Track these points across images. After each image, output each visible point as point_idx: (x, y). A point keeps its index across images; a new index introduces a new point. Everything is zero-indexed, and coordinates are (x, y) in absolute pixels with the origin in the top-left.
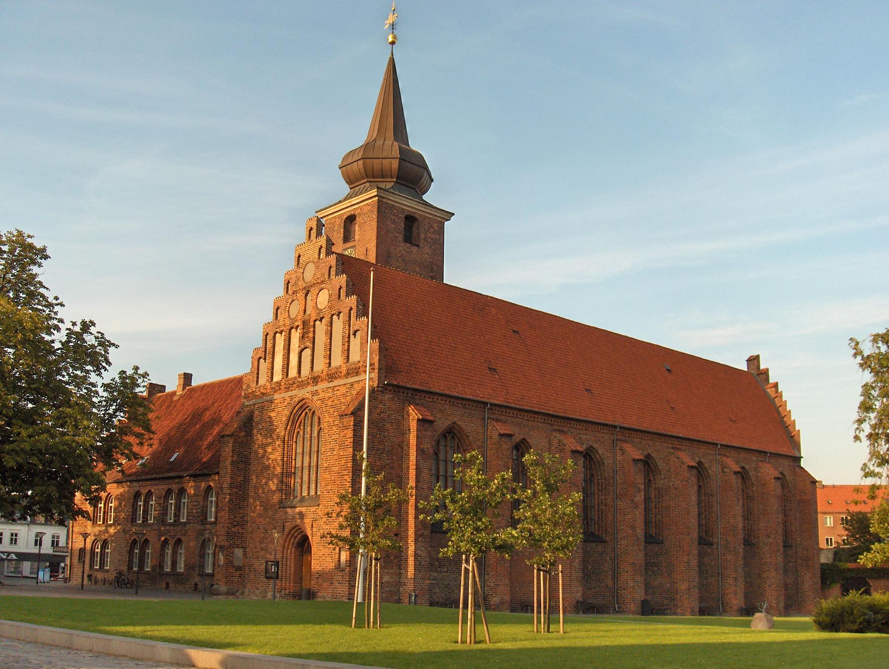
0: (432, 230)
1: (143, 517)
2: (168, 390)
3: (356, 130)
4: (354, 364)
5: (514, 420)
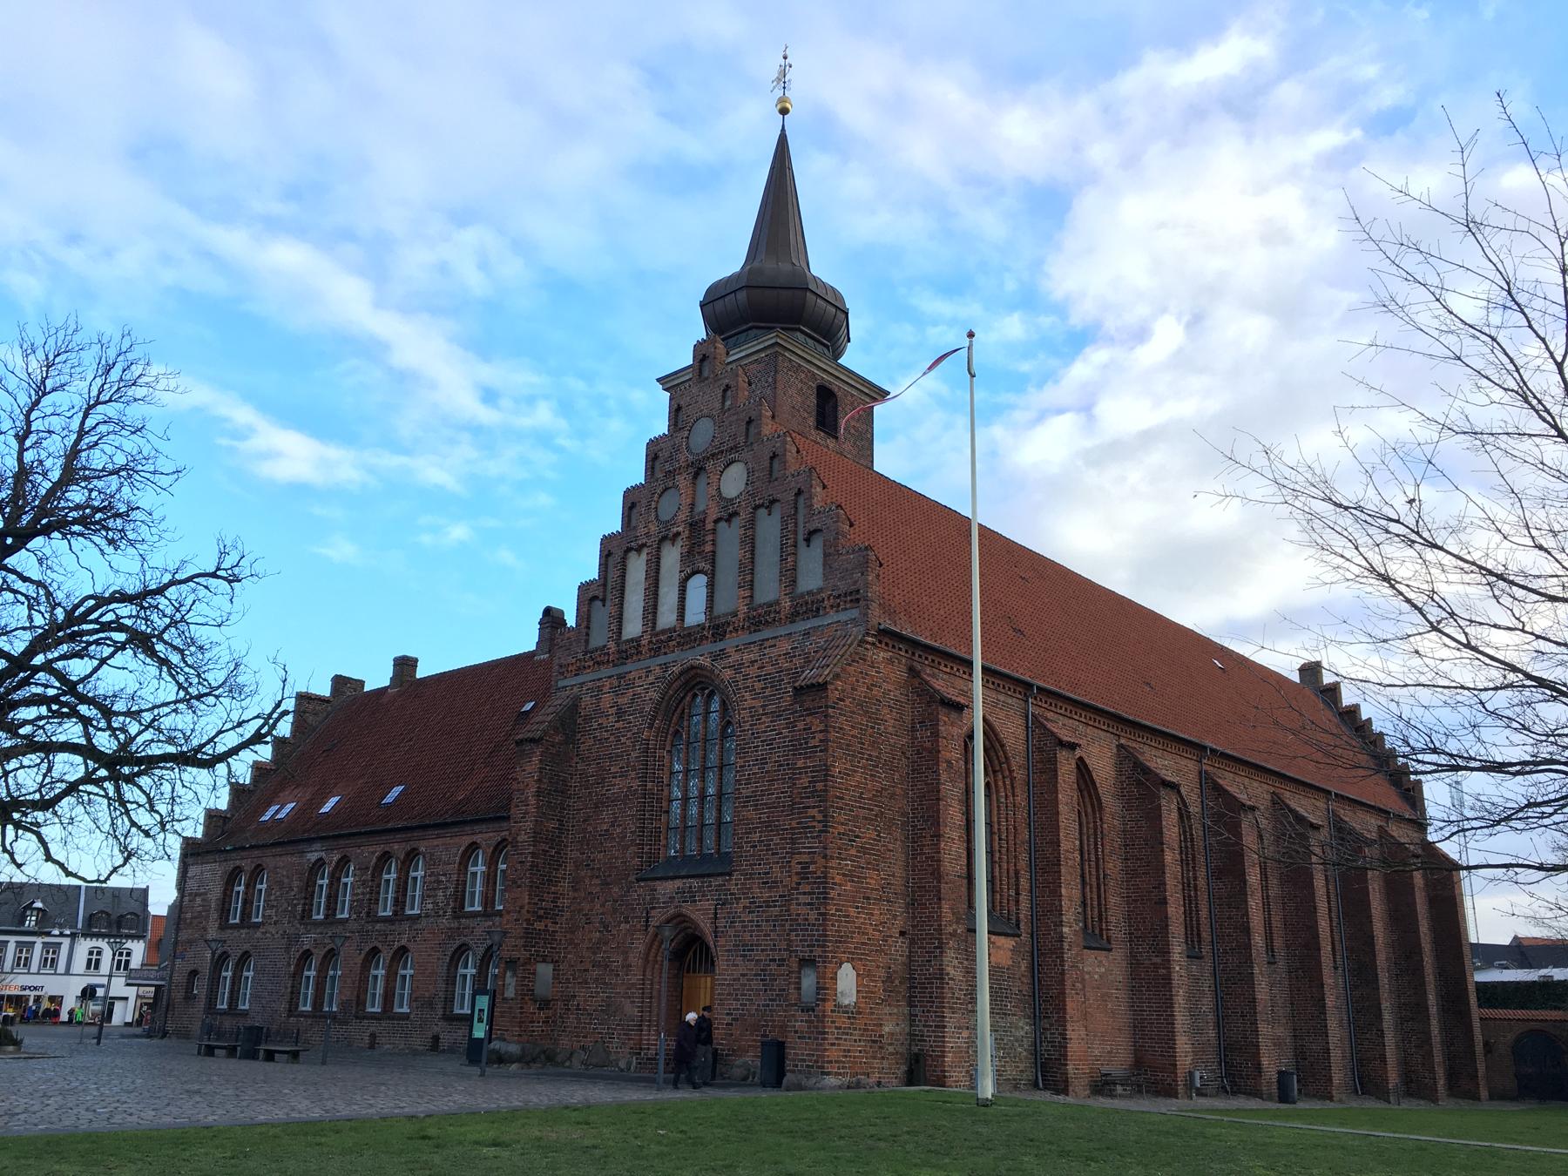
1: (328, 907)
3: (725, 250)
4: (810, 593)
5: (1067, 721)
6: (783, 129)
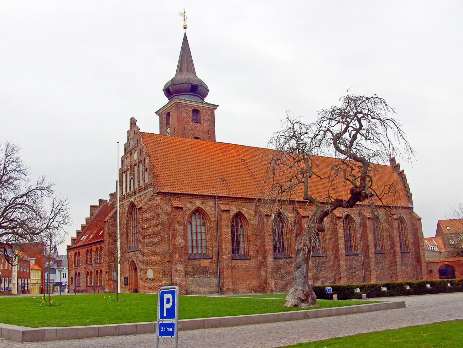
0: (208, 115)
3: (169, 72)
5: (233, 203)
6: (185, 33)
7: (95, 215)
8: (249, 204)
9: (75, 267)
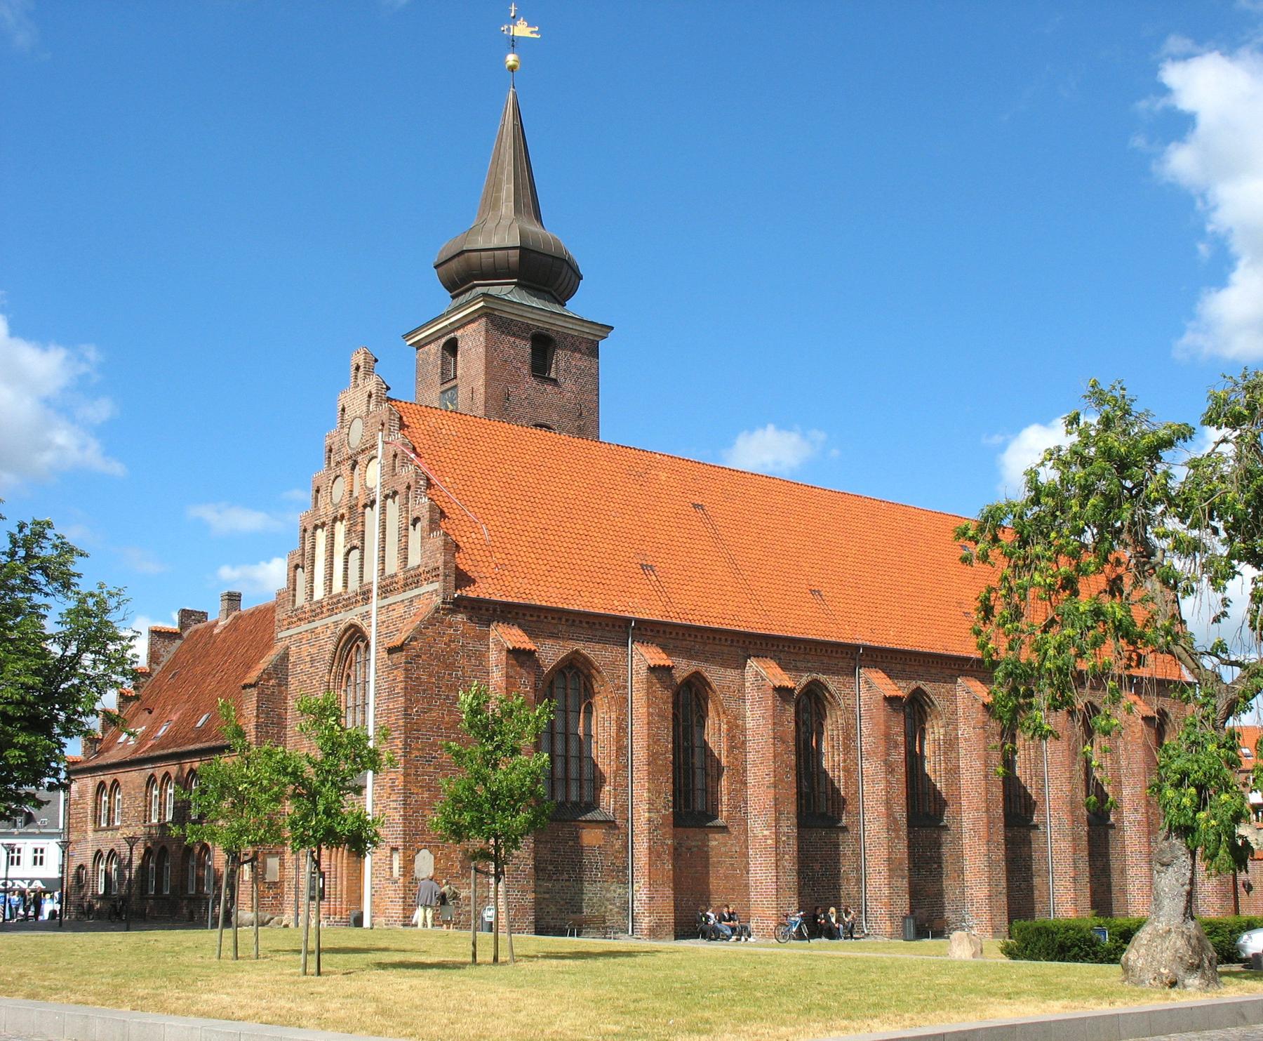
2: (211, 619)
4: (413, 569)
7: (165, 660)
8: (726, 650)
9: (95, 831)
